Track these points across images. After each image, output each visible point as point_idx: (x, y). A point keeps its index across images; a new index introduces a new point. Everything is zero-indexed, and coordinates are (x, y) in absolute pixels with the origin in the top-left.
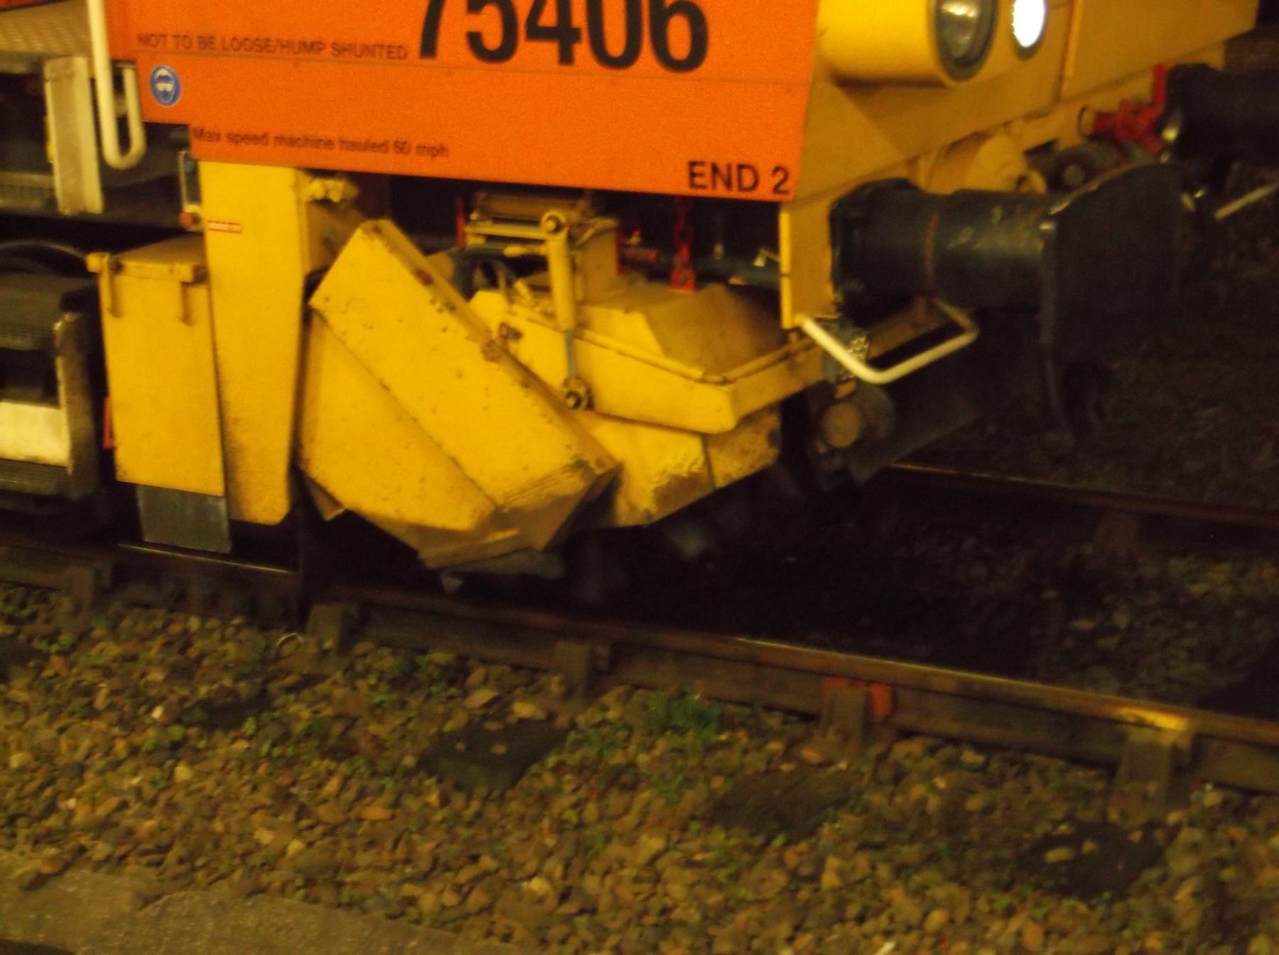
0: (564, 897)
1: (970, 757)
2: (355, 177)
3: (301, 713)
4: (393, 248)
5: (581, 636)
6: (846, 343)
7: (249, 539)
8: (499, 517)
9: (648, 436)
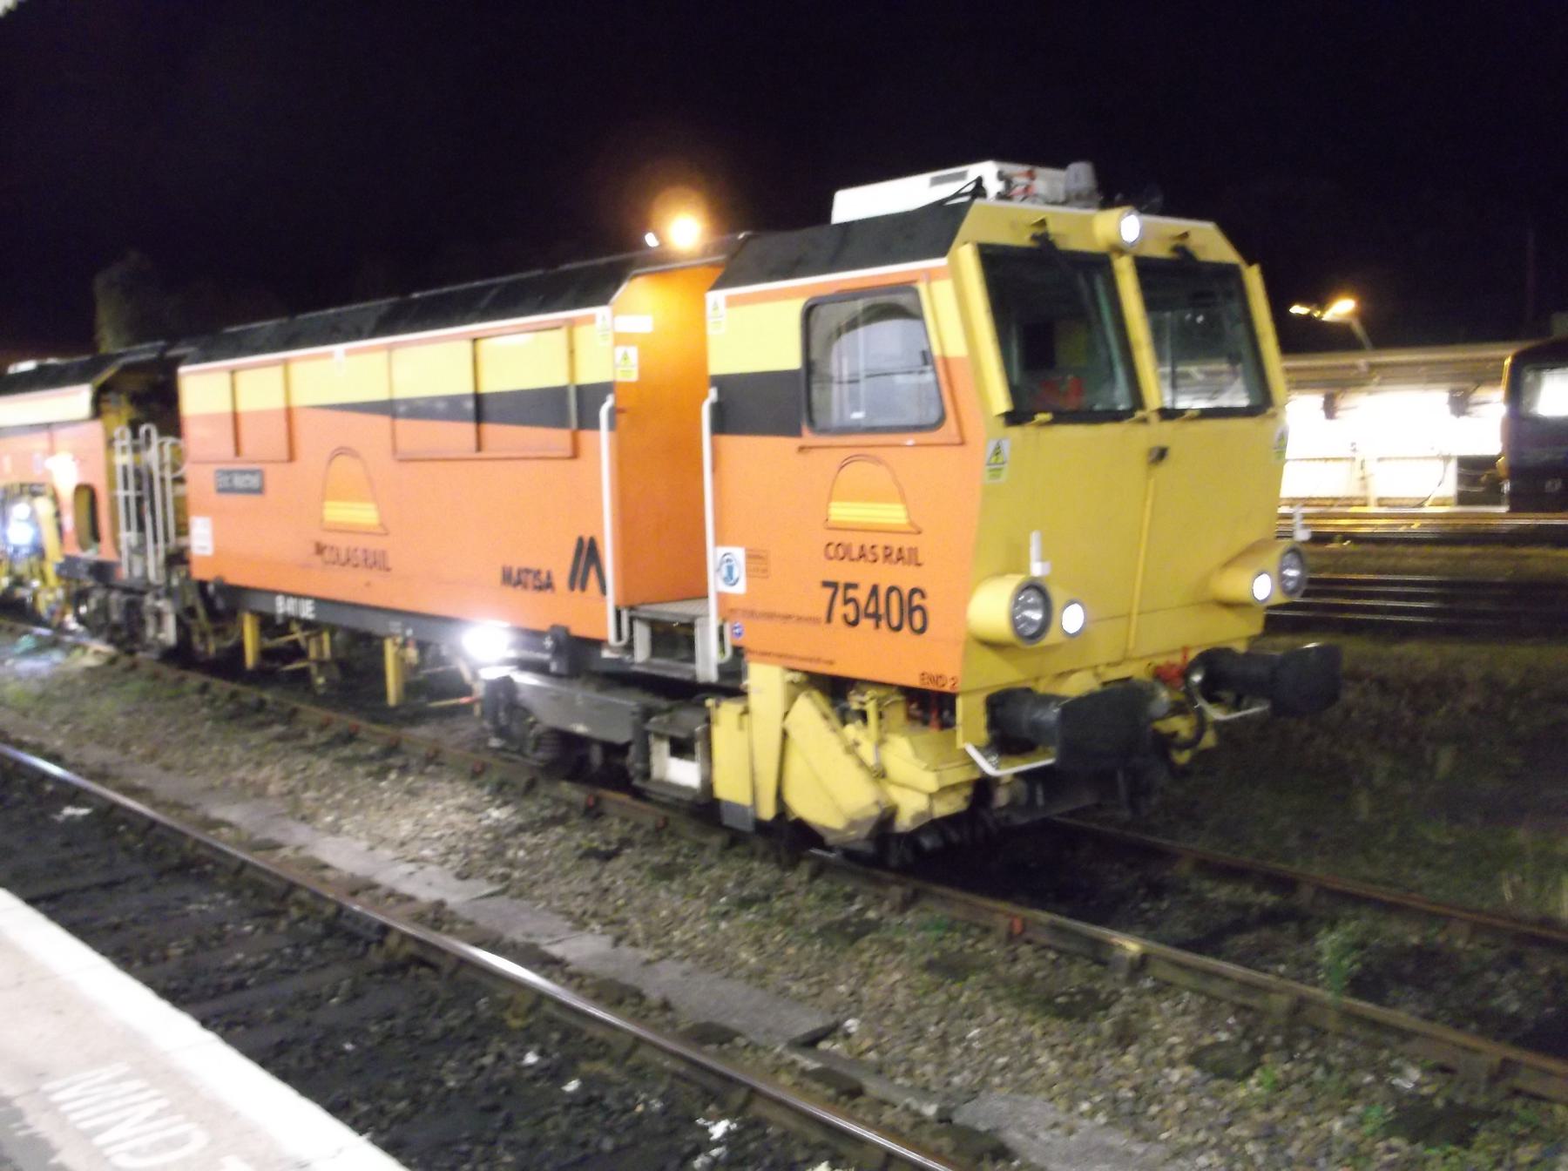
0: (852, 994)
1: (1051, 955)
2: (806, 673)
3: (778, 905)
4: (814, 702)
5: (901, 884)
6: (986, 757)
7: (761, 827)
8: (853, 824)
9: (909, 793)
